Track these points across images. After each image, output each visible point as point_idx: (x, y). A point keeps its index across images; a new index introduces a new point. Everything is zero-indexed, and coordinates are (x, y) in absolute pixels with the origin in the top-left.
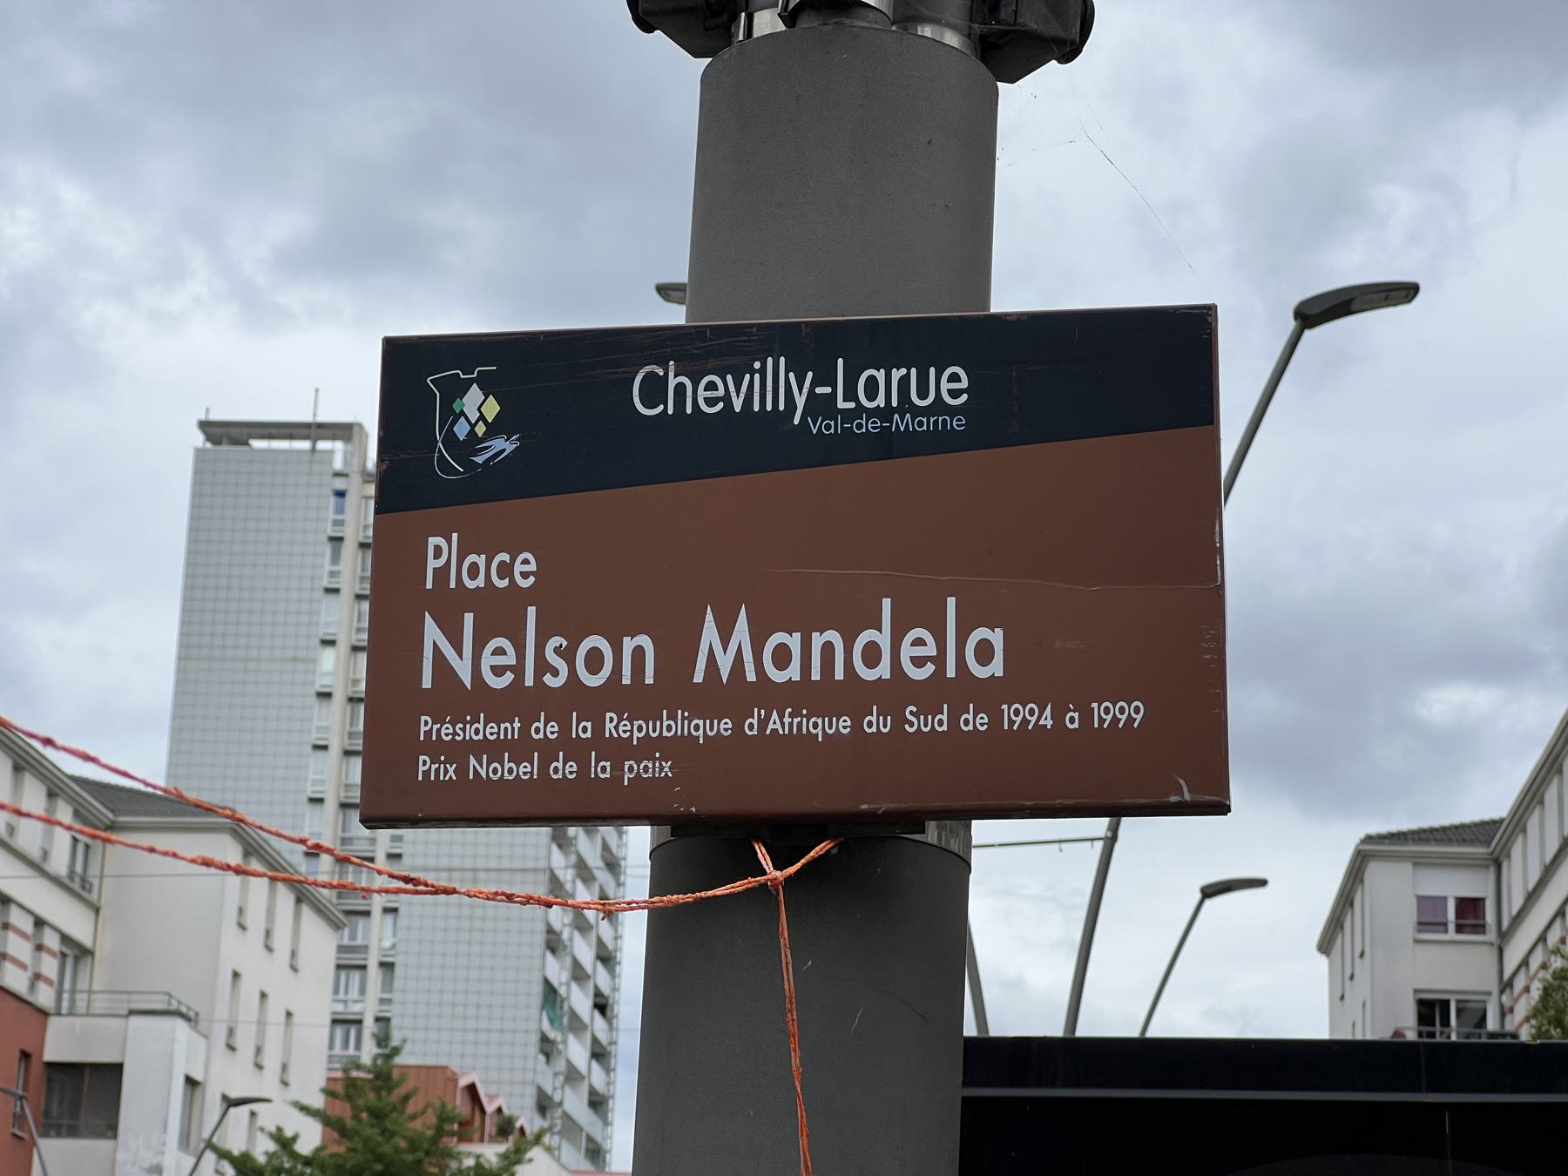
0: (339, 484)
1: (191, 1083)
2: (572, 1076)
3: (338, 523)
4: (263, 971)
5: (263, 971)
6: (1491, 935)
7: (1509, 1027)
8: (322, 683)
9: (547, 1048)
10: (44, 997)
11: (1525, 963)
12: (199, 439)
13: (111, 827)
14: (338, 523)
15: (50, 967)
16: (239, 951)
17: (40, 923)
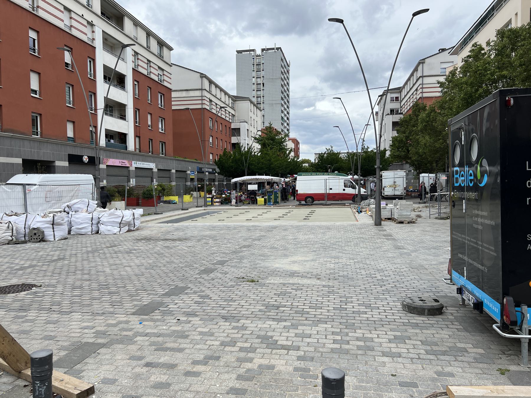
0: (253, 57)
1: (248, 130)
2: (285, 127)
3: (254, 62)
4: (254, 117)
5: (254, 117)
6: (399, 101)
7: (401, 112)
8: (253, 82)
9: (282, 124)
10: (231, 121)
11: (404, 104)
12: (236, 53)
13: (236, 101)
14: (254, 62)
15: (231, 117)
16: (251, 114)
17: (229, 112)
